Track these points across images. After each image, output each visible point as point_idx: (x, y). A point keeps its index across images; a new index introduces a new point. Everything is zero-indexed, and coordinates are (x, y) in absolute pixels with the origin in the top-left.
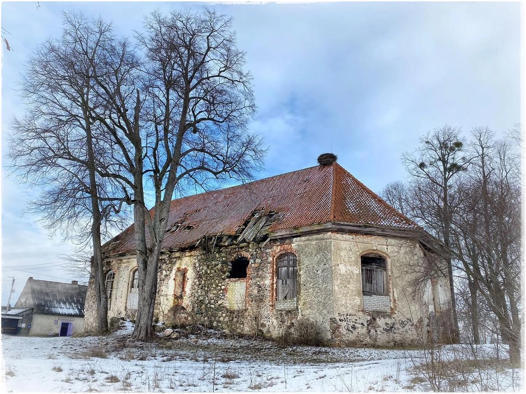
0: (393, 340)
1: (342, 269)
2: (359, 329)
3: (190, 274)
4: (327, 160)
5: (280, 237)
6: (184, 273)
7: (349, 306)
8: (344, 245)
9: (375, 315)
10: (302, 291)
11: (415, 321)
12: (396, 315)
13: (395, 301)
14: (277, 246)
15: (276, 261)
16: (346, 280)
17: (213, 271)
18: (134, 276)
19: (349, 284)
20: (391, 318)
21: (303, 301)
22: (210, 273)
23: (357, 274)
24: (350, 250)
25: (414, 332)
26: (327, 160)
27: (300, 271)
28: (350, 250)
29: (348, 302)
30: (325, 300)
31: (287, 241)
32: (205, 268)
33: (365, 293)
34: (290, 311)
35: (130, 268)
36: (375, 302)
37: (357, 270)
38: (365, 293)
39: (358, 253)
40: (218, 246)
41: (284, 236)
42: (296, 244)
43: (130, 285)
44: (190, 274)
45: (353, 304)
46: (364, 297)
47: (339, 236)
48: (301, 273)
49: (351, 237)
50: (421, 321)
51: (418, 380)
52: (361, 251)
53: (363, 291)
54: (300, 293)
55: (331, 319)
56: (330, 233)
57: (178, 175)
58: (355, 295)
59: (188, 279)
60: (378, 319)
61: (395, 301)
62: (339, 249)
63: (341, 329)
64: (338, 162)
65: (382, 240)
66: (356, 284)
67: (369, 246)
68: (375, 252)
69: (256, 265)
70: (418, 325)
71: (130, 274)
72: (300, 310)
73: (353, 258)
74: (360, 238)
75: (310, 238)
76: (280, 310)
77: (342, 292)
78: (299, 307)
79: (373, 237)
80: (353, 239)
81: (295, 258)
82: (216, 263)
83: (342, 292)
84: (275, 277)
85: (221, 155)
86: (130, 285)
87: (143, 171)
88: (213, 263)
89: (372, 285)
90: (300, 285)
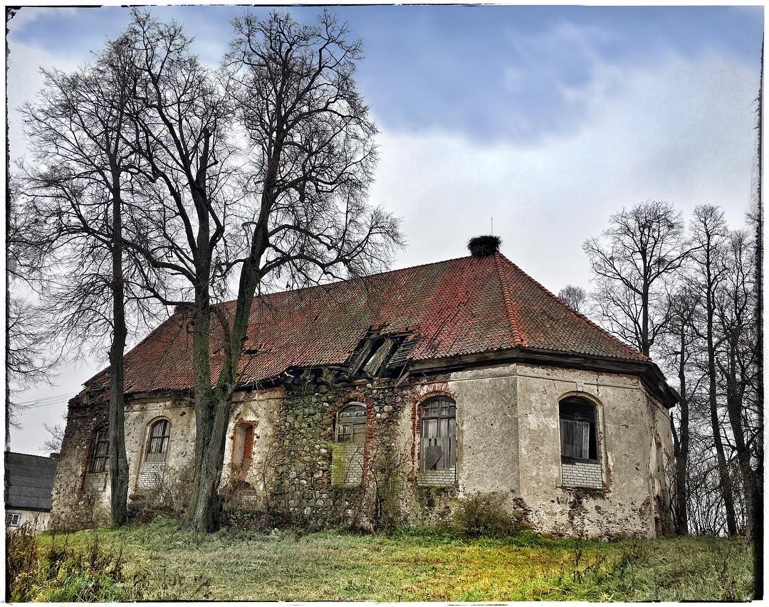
0: (607, 534)
1: (533, 421)
2: (557, 516)
3: (263, 430)
4: (485, 247)
5: (428, 371)
6: (248, 428)
7: (543, 480)
8: (536, 384)
9: (582, 492)
10: (466, 458)
11: (638, 505)
12: (611, 494)
13: (609, 471)
14: (423, 385)
15: (419, 410)
16: (538, 438)
17: (304, 425)
18: (152, 433)
19: (542, 445)
20: (604, 498)
21: (467, 472)
22: (301, 428)
23: (554, 429)
24: (545, 392)
25: (638, 521)
26: (485, 247)
27: (462, 425)
28: (545, 392)
29: (541, 473)
30: (504, 470)
31: (440, 377)
32: (290, 419)
33: (566, 460)
34: (443, 489)
35: (147, 419)
36: (583, 474)
37: (554, 423)
38: (566, 460)
39: (556, 397)
40: (317, 383)
41: (436, 370)
42: (455, 383)
43: (145, 448)
44: (263, 430)
45: (548, 476)
46: (564, 465)
47: (527, 370)
48: (464, 427)
49: (545, 371)
50: (647, 503)
51: (300, 535)
52: (560, 394)
53: (562, 457)
54: (461, 460)
55: (514, 500)
56: (513, 366)
57: (262, 264)
58: (552, 463)
59: (258, 438)
60: (584, 501)
61: (609, 471)
62: (529, 390)
63: (530, 516)
64: (503, 249)
65: (591, 377)
66: (554, 446)
67: (572, 387)
68: (580, 395)
69: (384, 416)
70: (643, 509)
71: (146, 429)
72: (460, 487)
73: (548, 405)
74: (560, 374)
75: (481, 372)
76: (427, 488)
77: (532, 458)
78: (460, 482)
79: (578, 372)
80: (548, 374)
81: (451, 404)
82: (312, 411)
83: (532, 458)
84: (416, 434)
85: (328, 237)
86: (145, 448)
87: (279, 255)
88: (307, 410)
89: (574, 447)
90: (461, 448)
